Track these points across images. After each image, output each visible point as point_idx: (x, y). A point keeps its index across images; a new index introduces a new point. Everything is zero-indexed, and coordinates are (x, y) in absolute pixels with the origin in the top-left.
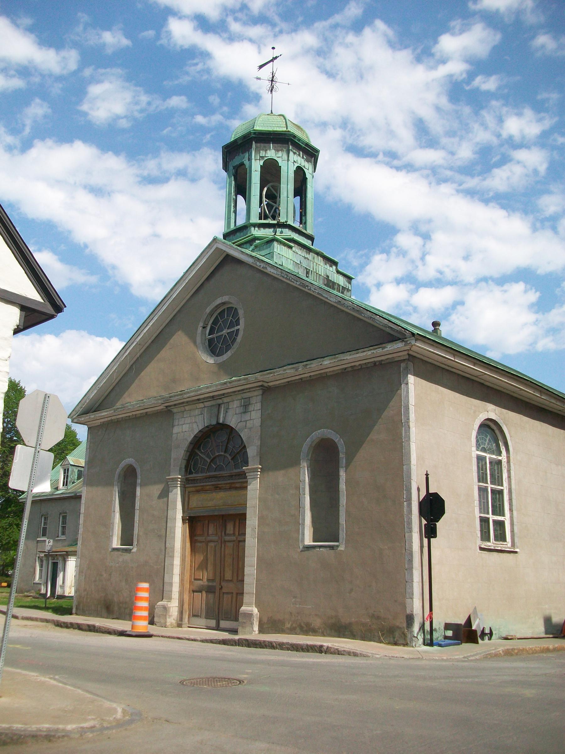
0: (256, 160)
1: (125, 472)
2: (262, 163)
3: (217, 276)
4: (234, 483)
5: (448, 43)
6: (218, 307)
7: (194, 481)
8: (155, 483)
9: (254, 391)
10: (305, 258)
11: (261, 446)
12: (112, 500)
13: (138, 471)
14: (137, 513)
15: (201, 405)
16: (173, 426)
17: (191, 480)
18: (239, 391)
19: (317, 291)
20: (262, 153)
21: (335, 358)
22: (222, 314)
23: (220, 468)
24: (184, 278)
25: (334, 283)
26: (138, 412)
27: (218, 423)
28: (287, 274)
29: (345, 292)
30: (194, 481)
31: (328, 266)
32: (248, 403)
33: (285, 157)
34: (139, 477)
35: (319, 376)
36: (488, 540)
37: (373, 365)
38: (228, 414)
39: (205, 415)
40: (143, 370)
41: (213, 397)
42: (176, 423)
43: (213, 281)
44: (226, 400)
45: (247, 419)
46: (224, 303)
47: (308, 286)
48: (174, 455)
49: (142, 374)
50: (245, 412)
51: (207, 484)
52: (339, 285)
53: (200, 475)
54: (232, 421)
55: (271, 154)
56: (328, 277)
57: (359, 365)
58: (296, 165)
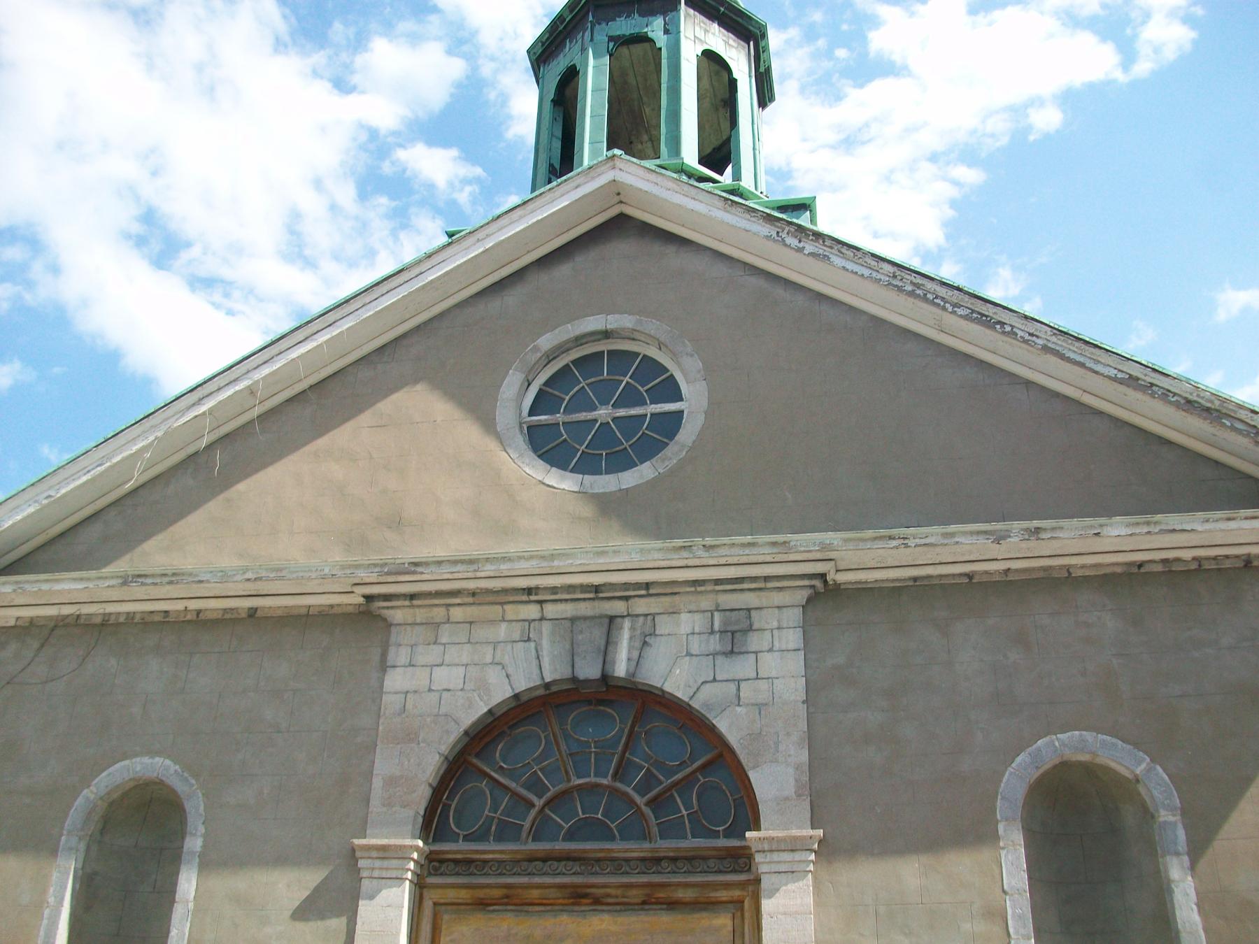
1: (111, 804)
3: (582, 261)
4: (662, 886)
5: (386, 57)
6: (579, 340)
7: (466, 865)
8: (281, 860)
9: (780, 589)
11: (815, 766)
12: (39, 904)
13: (196, 808)
15: (532, 611)
16: (384, 667)
17: (456, 862)
18: (718, 582)
19: (1040, 342)
21: (1148, 523)
22: (588, 363)
23: (601, 831)
24: (480, 235)
26: (213, 604)
27: (605, 678)
28: (919, 280)
30: (466, 865)
32: (744, 625)
35: (1041, 574)
37: (1242, 564)
38: (650, 653)
39: (545, 643)
40: (247, 476)
41: (597, 589)
42: (399, 655)
43: (564, 270)
44: (641, 606)
45: (740, 675)
46: (607, 334)
47: (1002, 324)
48: (385, 765)
49: (241, 486)
50: (732, 652)
51: (537, 880)
53: (492, 849)
57: (1194, 559)
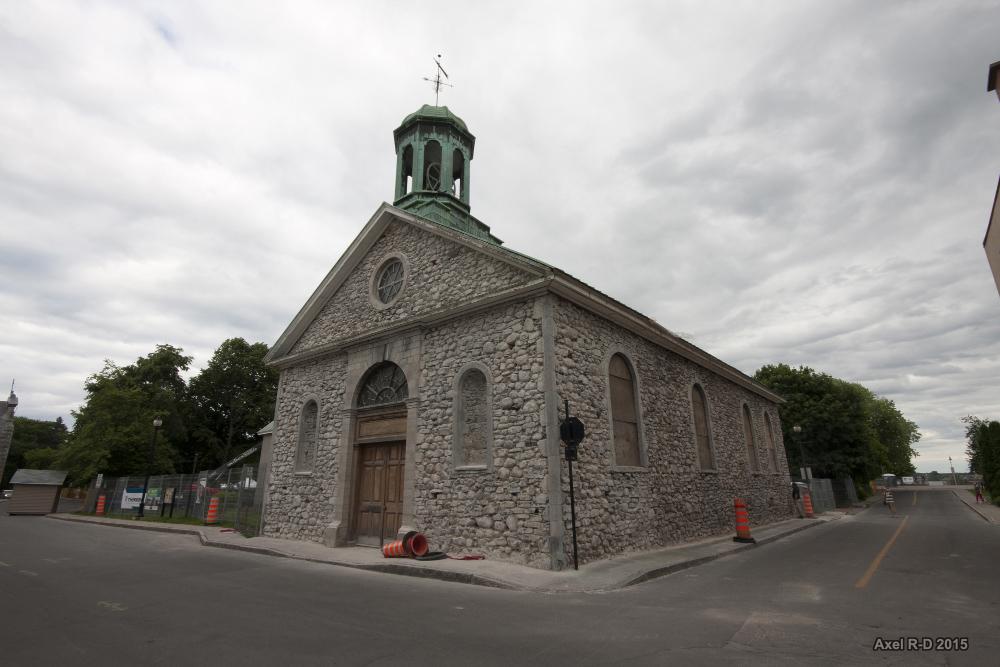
2: (425, 143)
20: (426, 135)
33: (446, 139)
55: (434, 136)
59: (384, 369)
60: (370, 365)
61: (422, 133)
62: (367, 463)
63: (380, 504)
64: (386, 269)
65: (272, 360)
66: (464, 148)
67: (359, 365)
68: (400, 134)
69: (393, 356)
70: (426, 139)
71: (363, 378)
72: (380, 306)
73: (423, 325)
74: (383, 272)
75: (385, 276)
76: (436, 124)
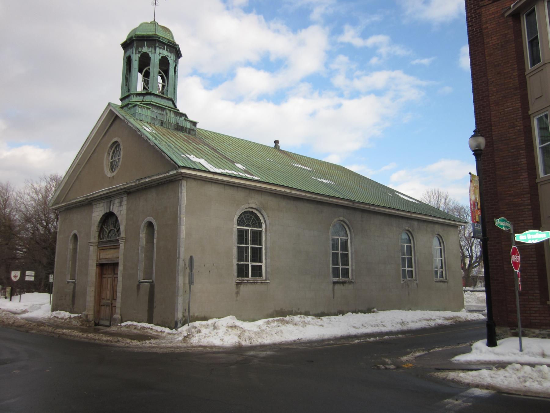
0: (136, 53)
2: (139, 55)
3: (114, 125)
10: (160, 114)
14: (77, 261)
20: (140, 49)
25: (182, 127)
29: (191, 132)
31: (178, 118)
33: (153, 51)
34: (79, 241)
36: (338, 277)
52: (186, 128)
54: (115, 212)
55: (145, 49)
56: (178, 124)
58: (161, 55)
59: (109, 218)
60: (103, 214)
61: (137, 48)
62: (104, 276)
63: (109, 301)
64: (114, 147)
65: (53, 205)
66: (169, 54)
67: (98, 212)
68: (126, 46)
69: (114, 209)
70: (140, 52)
71: (100, 222)
72: (109, 174)
73: (128, 191)
74: (115, 146)
75: (113, 153)
76: (147, 40)
